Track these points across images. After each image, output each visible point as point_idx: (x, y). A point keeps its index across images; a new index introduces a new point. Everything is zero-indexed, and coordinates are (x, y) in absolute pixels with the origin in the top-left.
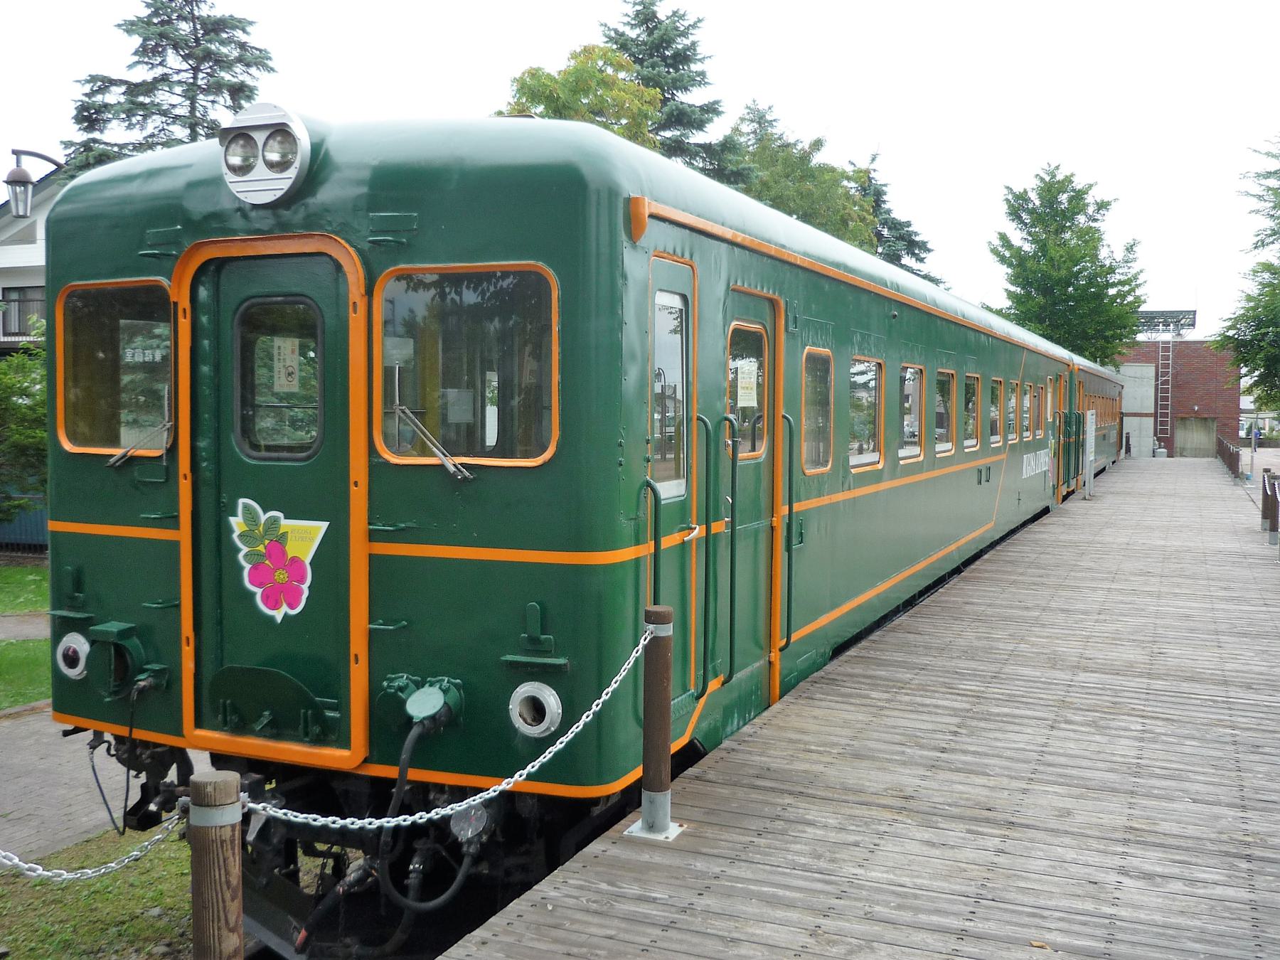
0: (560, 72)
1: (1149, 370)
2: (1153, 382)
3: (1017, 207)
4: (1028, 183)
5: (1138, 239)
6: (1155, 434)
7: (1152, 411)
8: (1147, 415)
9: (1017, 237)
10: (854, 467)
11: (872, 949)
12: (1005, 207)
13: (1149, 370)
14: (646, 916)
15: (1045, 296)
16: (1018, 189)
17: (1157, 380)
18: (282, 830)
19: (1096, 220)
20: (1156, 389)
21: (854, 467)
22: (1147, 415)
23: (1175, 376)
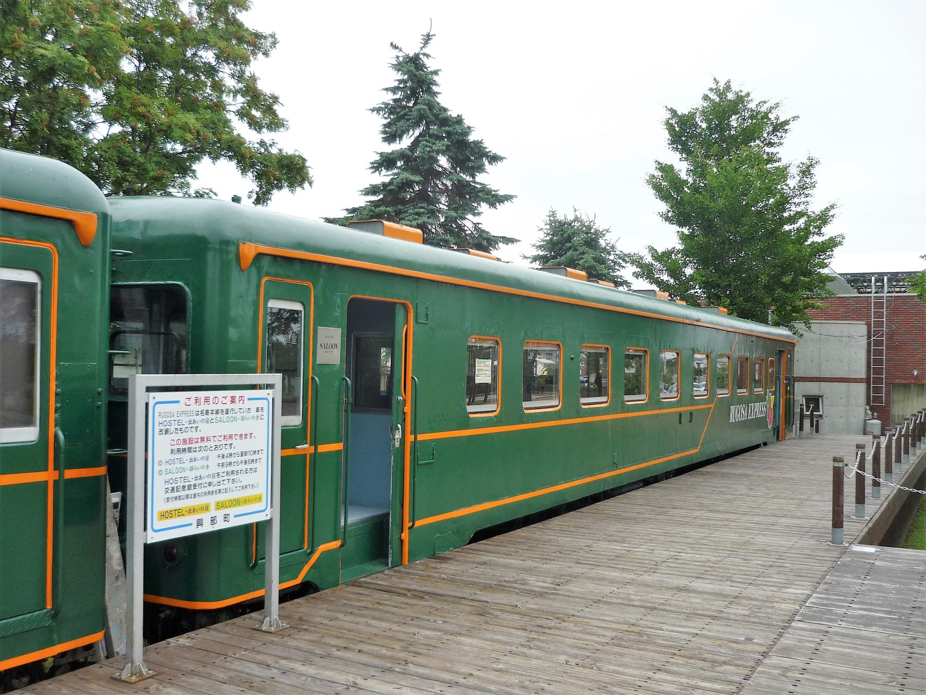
0: (239, 135)
1: (860, 329)
2: (864, 341)
3: (682, 131)
4: (690, 100)
5: (816, 155)
6: (868, 403)
7: (863, 375)
8: (856, 381)
9: (682, 167)
10: (527, 409)
11: (483, 612)
12: (666, 135)
13: (860, 329)
14: (308, 360)
15: (706, 235)
16: (683, 110)
17: (869, 337)
18: (184, 370)
19: (771, 144)
20: (869, 351)
21: (527, 409)
22: (856, 381)
23: (891, 335)
